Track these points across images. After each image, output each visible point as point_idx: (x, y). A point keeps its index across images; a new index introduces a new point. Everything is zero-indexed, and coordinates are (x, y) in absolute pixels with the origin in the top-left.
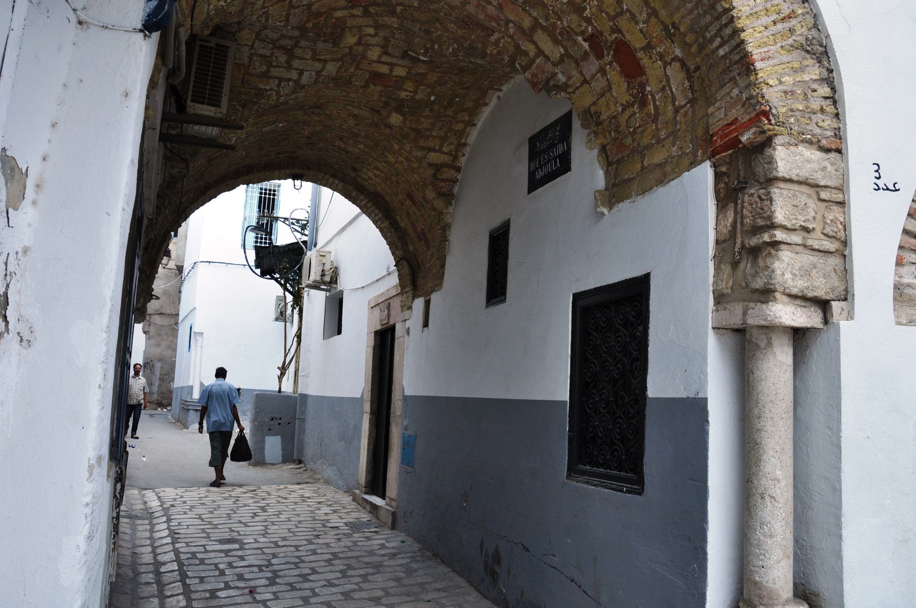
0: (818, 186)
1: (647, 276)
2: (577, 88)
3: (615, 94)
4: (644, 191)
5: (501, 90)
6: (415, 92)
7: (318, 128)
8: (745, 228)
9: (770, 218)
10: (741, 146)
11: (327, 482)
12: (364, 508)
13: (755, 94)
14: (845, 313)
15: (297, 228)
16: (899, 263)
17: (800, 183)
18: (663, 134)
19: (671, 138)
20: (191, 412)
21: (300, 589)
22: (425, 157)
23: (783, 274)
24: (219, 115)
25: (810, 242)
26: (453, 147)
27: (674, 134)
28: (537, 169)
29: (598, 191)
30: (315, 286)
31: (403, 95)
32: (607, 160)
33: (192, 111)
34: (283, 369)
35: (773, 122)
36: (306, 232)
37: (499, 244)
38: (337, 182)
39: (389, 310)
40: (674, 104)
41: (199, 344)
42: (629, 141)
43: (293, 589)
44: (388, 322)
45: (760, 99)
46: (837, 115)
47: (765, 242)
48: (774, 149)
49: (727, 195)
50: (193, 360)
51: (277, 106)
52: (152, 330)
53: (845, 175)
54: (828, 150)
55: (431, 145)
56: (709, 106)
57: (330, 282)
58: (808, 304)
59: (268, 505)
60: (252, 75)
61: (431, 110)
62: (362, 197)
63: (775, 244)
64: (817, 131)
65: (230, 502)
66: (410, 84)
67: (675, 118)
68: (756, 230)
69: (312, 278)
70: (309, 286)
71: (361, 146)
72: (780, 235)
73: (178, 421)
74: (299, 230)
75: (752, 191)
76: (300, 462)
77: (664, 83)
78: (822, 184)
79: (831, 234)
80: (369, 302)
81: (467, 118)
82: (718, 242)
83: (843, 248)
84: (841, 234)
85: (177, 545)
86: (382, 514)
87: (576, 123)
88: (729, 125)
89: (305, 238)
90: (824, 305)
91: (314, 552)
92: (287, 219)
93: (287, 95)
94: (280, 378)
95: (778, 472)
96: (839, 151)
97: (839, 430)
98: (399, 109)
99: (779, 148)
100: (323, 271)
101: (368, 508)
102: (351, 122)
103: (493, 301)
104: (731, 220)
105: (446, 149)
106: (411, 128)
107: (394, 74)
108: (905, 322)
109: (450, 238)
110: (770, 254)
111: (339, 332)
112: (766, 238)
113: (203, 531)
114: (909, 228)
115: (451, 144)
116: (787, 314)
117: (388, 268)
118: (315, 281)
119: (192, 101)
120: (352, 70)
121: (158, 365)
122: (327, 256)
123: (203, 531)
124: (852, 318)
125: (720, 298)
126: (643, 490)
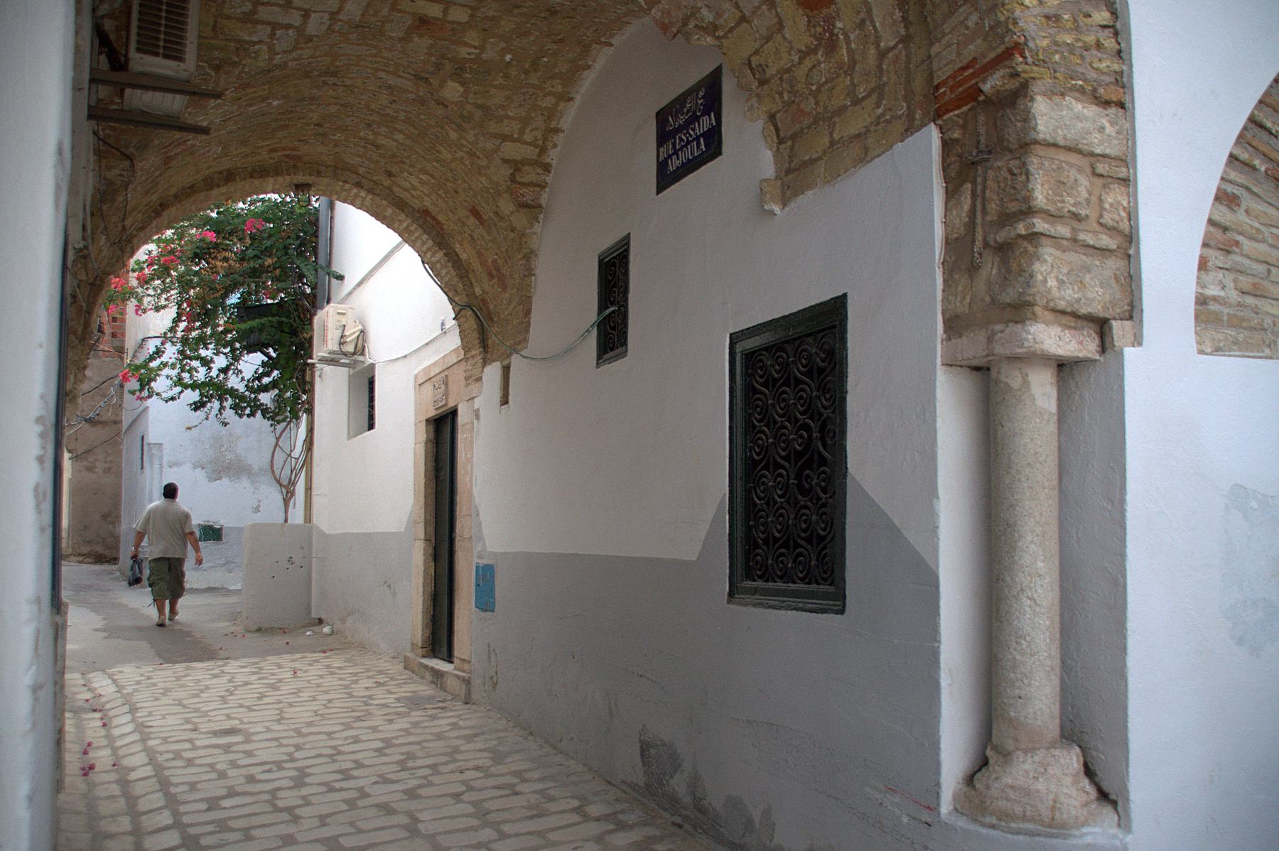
0: (1092, 154)
1: (845, 295)
2: (731, 31)
3: (788, 36)
4: (833, 176)
5: (611, 45)
6: (482, 48)
7: (333, 109)
8: (989, 218)
9: (1027, 199)
10: (982, 98)
12: (423, 677)
13: (1002, 19)
14: (1130, 337)
16: (1203, 265)
17: (1069, 149)
18: (861, 92)
19: (874, 96)
21: (341, 790)
22: (497, 150)
23: (1045, 281)
24: (184, 75)
25: (1082, 236)
26: (538, 134)
27: (879, 90)
28: (670, 156)
29: (765, 180)
30: (331, 361)
31: (464, 52)
32: (778, 135)
33: (139, 69)
35: (1030, 60)
37: (613, 273)
38: (363, 194)
40: (878, 46)
42: (809, 105)
43: (332, 790)
45: (1011, 27)
46: (1119, 52)
47: (1020, 236)
48: (1032, 100)
49: (962, 169)
51: (269, 71)
53: (1129, 136)
54: (1106, 104)
55: (507, 131)
56: (931, 44)
58: (1080, 323)
59: (280, 681)
60: (229, 18)
61: (506, 76)
62: (402, 217)
63: (1033, 237)
64: (1092, 75)
65: (224, 680)
66: (475, 35)
67: (879, 67)
68: (1007, 219)
71: (400, 137)
72: (1040, 225)
75: (999, 164)
77: (862, 15)
78: (1098, 151)
79: (1111, 223)
80: (416, 377)
81: (560, 89)
82: (948, 242)
83: (1127, 242)
84: (1125, 226)
85: (151, 743)
86: (451, 683)
87: (728, 85)
88: (963, 69)
90: (1101, 326)
91: (357, 740)
93: (284, 52)
95: (1041, 564)
96: (1121, 105)
97: (1123, 501)
98: (458, 73)
99: (1039, 98)
101: (428, 676)
102: (384, 98)
103: (607, 356)
104: (966, 207)
105: (528, 137)
106: (478, 106)
107: (450, 18)
108: (1209, 350)
109: (537, 271)
110: (1026, 251)
111: (371, 426)
112: (1021, 229)
113: (188, 721)
114: (1216, 217)
115: (537, 129)
116: (1050, 338)
117: (443, 324)
119: (138, 50)
120: (385, 12)
123: (188, 721)
124: (1140, 344)
125: (954, 326)
126: (844, 606)
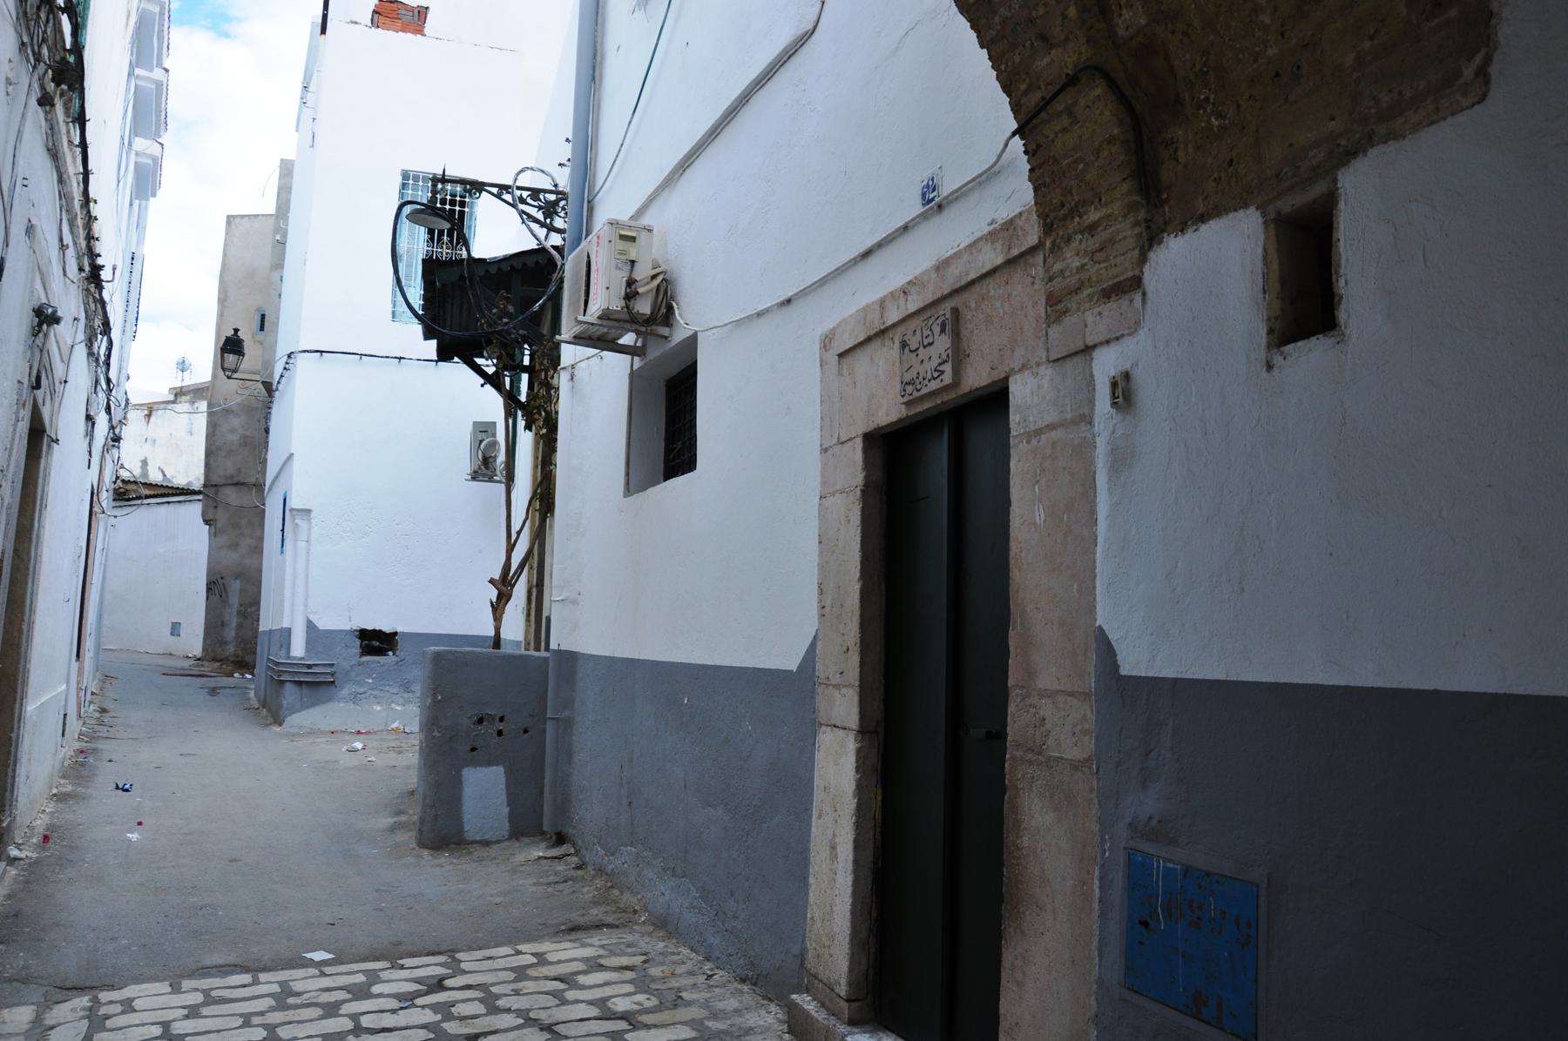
11: (663, 925)
15: (533, 211)
20: (288, 685)
30: (599, 339)
34: (504, 585)
36: (559, 223)
39: (956, 335)
41: (303, 536)
44: (956, 383)
50: (288, 570)
52: (222, 517)
57: (650, 320)
69: (595, 308)
70: (579, 340)
73: (264, 705)
74: (540, 216)
76: (561, 839)
89: (556, 240)
92: (504, 188)
94: (498, 608)
100: (631, 282)
118: (606, 316)
121: (235, 586)
122: (643, 238)
